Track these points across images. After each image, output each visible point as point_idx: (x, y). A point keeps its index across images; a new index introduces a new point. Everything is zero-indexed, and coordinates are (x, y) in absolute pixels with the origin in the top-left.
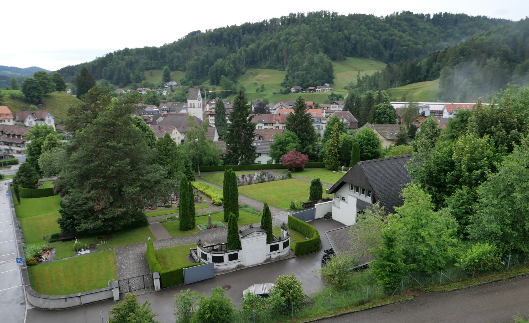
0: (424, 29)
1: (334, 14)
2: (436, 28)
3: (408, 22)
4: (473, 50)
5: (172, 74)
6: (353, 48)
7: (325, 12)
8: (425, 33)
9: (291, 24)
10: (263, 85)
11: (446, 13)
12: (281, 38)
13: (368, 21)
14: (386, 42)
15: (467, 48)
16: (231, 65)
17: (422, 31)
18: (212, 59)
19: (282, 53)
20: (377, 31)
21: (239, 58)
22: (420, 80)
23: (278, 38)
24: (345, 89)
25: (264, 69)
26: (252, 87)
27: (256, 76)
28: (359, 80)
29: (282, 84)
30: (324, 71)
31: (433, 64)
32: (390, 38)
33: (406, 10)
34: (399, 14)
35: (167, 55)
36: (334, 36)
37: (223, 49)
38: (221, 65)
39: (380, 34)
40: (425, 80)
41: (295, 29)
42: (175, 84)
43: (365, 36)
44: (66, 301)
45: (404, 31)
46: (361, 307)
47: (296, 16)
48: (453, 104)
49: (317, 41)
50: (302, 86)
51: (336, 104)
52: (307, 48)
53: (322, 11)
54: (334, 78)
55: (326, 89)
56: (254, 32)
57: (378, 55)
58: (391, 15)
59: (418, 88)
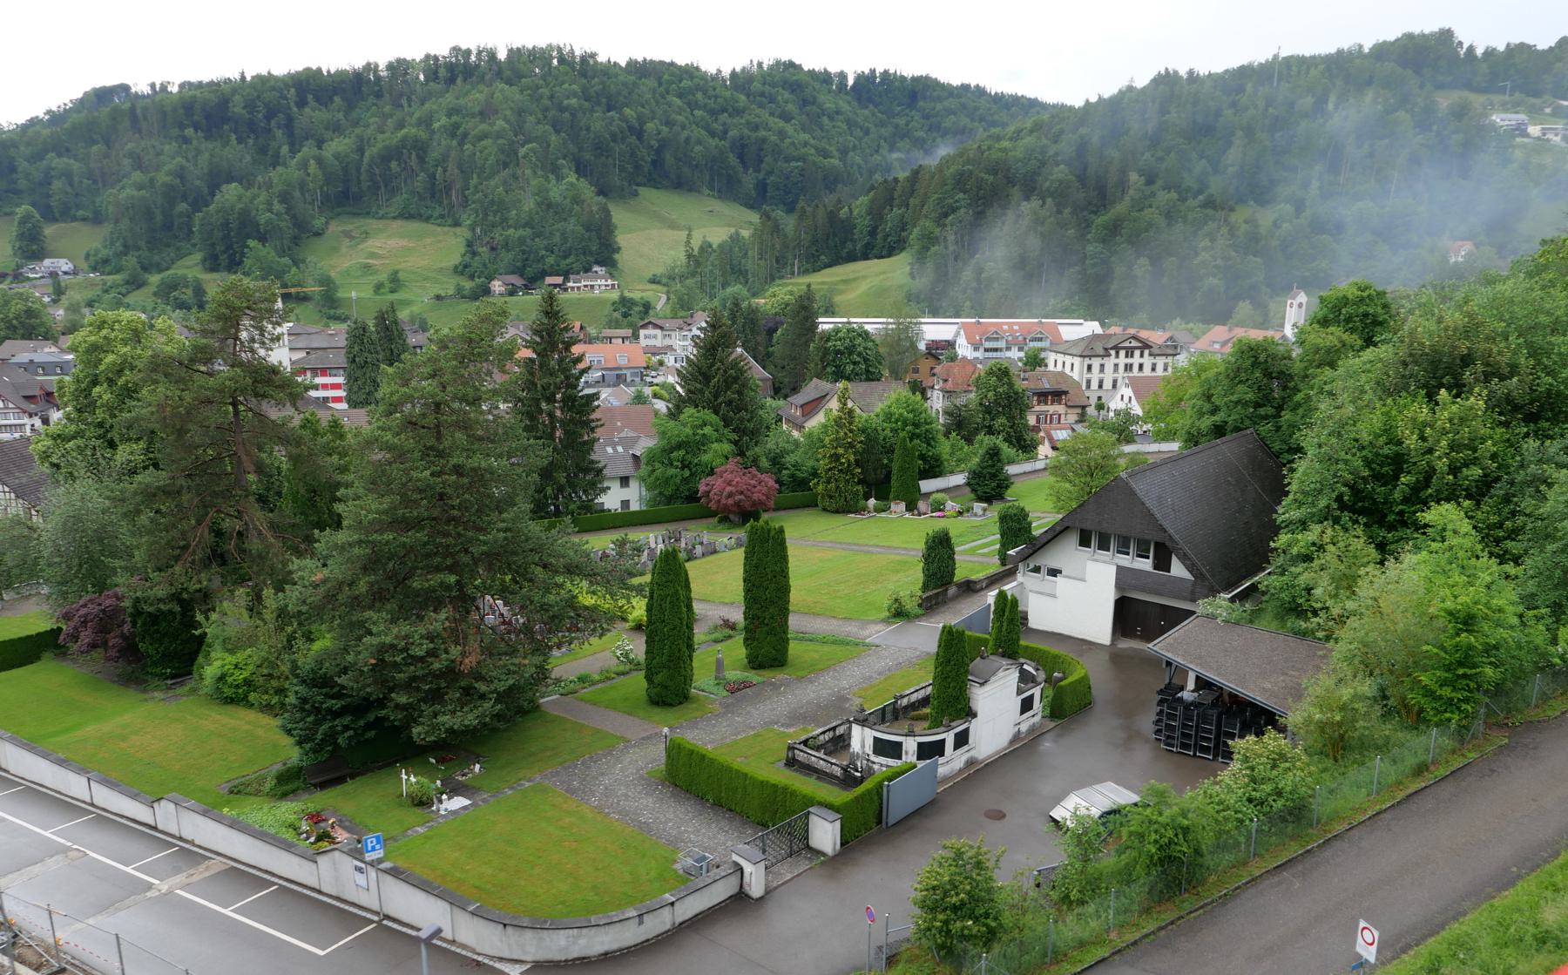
0: (838, 113)
1: (588, 58)
2: (866, 112)
3: (793, 91)
4: (986, 177)
5: (49, 230)
6: (654, 163)
7: (559, 49)
8: (840, 124)
9: (459, 81)
10: (396, 272)
11: (886, 72)
12: (436, 125)
13: (686, 83)
14: (743, 146)
15: (971, 172)
16: (277, 206)
17: (831, 118)
18: (198, 183)
19: (445, 171)
20: (713, 113)
21: (302, 185)
22: (851, 258)
23: (427, 122)
24: (654, 281)
25: (388, 222)
26: (357, 277)
27: (364, 241)
28: (689, 256)
29: (456, 267)
30: (588, 229)
31: (886, 211)
32: (754, 135)
33: (785, 58)
34: (765, 67)
35: (23, 165)
36: (598, 122)
37: (235, 153)
38: (240, 206)
39: (725, 124)
40: (866, 257)
41: (476, 97)
42: (65, 268)
43: (683, 127)
44: (641, 923)
45: (787, 118)
46: (1428, 779)
47: (473, 58)
48: (979, 323)
49: (553, 138)
50: (521, 276)
51: (656, 326)
52: (524, 157)
53: (550, 45)
54: (618, 250)
55: (599, 282)
56: (337, 99)
57: (726, 186)
58: (744, 69)
59: (855, 279)
